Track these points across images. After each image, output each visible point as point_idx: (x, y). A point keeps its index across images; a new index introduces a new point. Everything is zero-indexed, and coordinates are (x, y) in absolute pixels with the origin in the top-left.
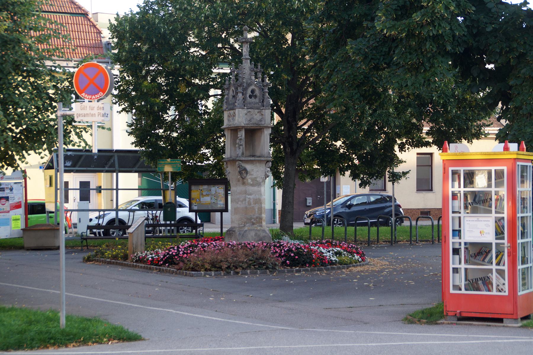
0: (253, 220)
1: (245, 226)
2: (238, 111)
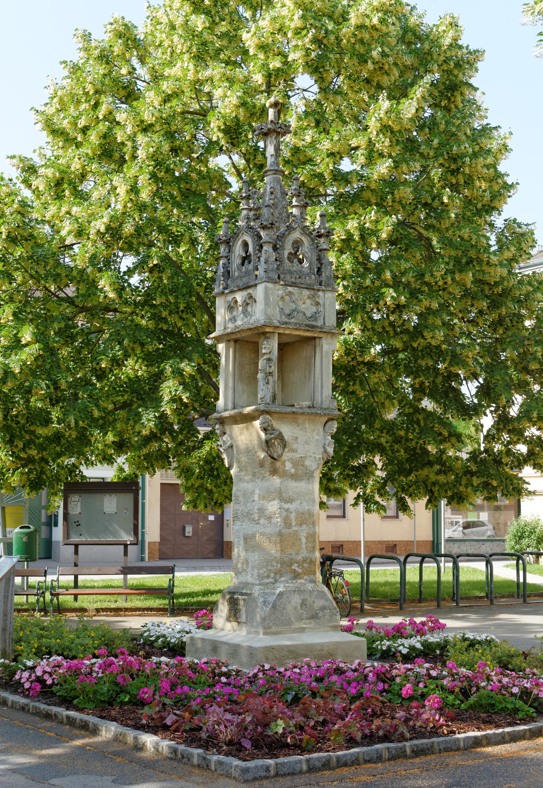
0: (295, 567)
1: (276, 581)
2: (266, 288)
